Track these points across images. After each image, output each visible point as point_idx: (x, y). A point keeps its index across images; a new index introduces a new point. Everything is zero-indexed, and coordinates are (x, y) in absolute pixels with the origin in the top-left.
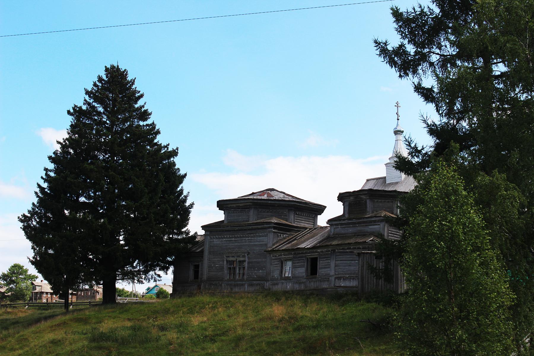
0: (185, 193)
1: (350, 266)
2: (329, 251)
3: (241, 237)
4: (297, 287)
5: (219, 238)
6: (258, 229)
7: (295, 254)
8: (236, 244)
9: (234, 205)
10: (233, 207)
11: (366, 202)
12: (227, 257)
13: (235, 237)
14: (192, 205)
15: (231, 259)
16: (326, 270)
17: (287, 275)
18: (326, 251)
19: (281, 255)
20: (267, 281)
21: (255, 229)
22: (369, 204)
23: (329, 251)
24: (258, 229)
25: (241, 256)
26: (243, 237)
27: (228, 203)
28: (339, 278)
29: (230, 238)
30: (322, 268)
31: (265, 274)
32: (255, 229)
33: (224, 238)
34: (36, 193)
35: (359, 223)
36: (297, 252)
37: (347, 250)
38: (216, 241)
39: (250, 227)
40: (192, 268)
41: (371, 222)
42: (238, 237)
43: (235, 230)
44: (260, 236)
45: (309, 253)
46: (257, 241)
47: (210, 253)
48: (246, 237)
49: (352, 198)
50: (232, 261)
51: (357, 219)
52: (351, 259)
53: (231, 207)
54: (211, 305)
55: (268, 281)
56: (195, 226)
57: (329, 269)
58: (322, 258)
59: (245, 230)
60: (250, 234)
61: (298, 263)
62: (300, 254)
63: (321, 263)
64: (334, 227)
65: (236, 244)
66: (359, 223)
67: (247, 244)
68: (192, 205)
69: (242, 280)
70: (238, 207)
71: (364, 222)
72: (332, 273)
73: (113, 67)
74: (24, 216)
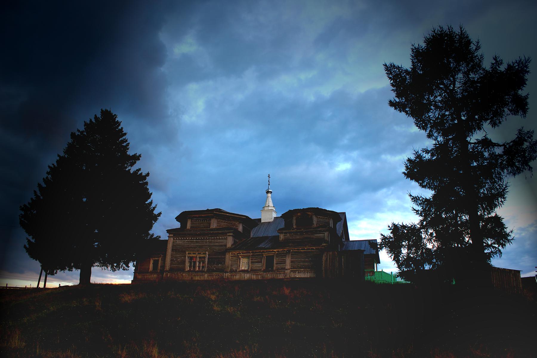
0: (153, 205)
3: (201, 239)
5: (181, 239)
8: (197, 244)
11: (312, 217)
13: (196, 239)
14: (160, 214)
16: (281, 265)
17: (243, 269)
26: (204, 239)
29: (191, 239)
33: (186, 239)
34: (35, 192)
38: (179, 242)
40: (152, 262)
42: (199, 239)
47: (173, 250)
50: (192, 257)
54: (486, 213)
56: (159, 231)
65: (197, 244)
68: (160, 214)
69: (202, 271)
73: (107, 111)
74: (25, 206)
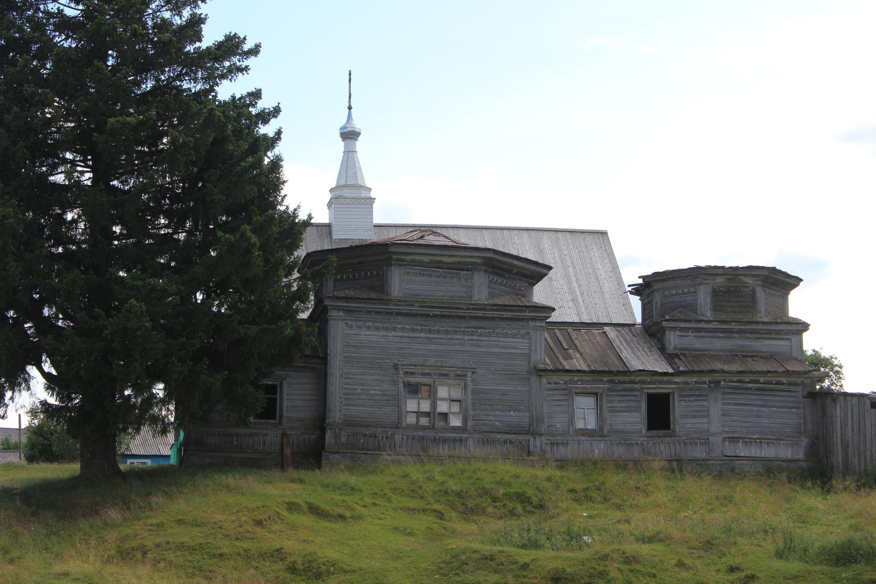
1: (759, 416)
2: (705, 383)
4: (620, 451)
6: (502, 319)
7: (611, 381)
8: (432, 347)
9: (426, 259)
10: (422, 262)
11: (754, 291)
12: (406, 373)
15: (412, 380)
18: (696, 383)
19: (572, 382)
20: (535, 434)
21: (492, 319)
22: (761, 295)
23: (705, 383)
24: (502, 319)
25: (452, 375)
27: (780, 277)
28: (733, 440)
30: (685, 416)
31: (527, 420)
32: (492, 319)
33: (395, 329)
35: (740, 332)
36: (616, 379)
37: (750, 385)
39: (480, 313)
41: (769, 332)
43: (428, 316)
44: (506, 336)
45: (650, 383)
46: (497, 346)
48: (464, 333)
49: (720, 280)
51: (738, 322)
52: (761, 403)
53: (413, 261)
55: (541, 435)
57: (706, 420)
58: (685, 396)
59: (463, 317)
60: (477, 328)
61: (619, 401)
62: (625, 382)
63: (678, 408)
64: (678, 333)
65: (432, 347)
66: (740, 332)
67: (466, 348)
70: (439, 265)
71: (752, 332)
72: (715, 427)
